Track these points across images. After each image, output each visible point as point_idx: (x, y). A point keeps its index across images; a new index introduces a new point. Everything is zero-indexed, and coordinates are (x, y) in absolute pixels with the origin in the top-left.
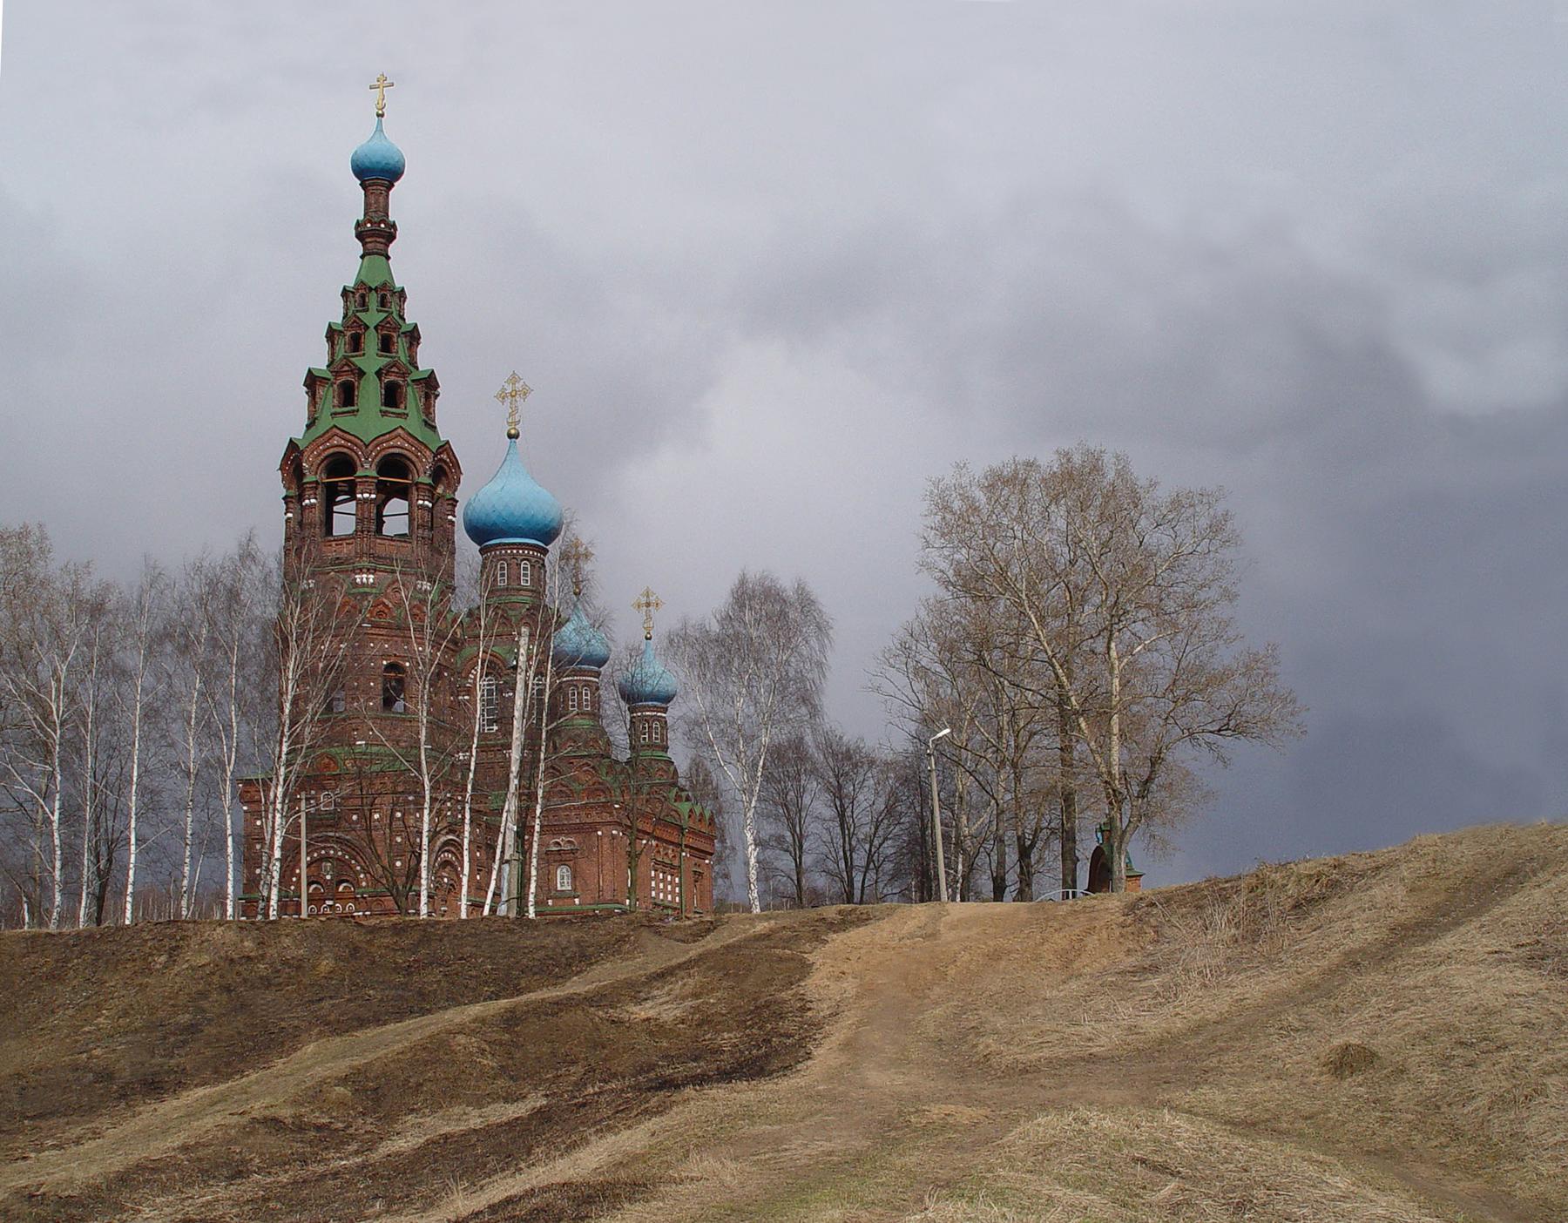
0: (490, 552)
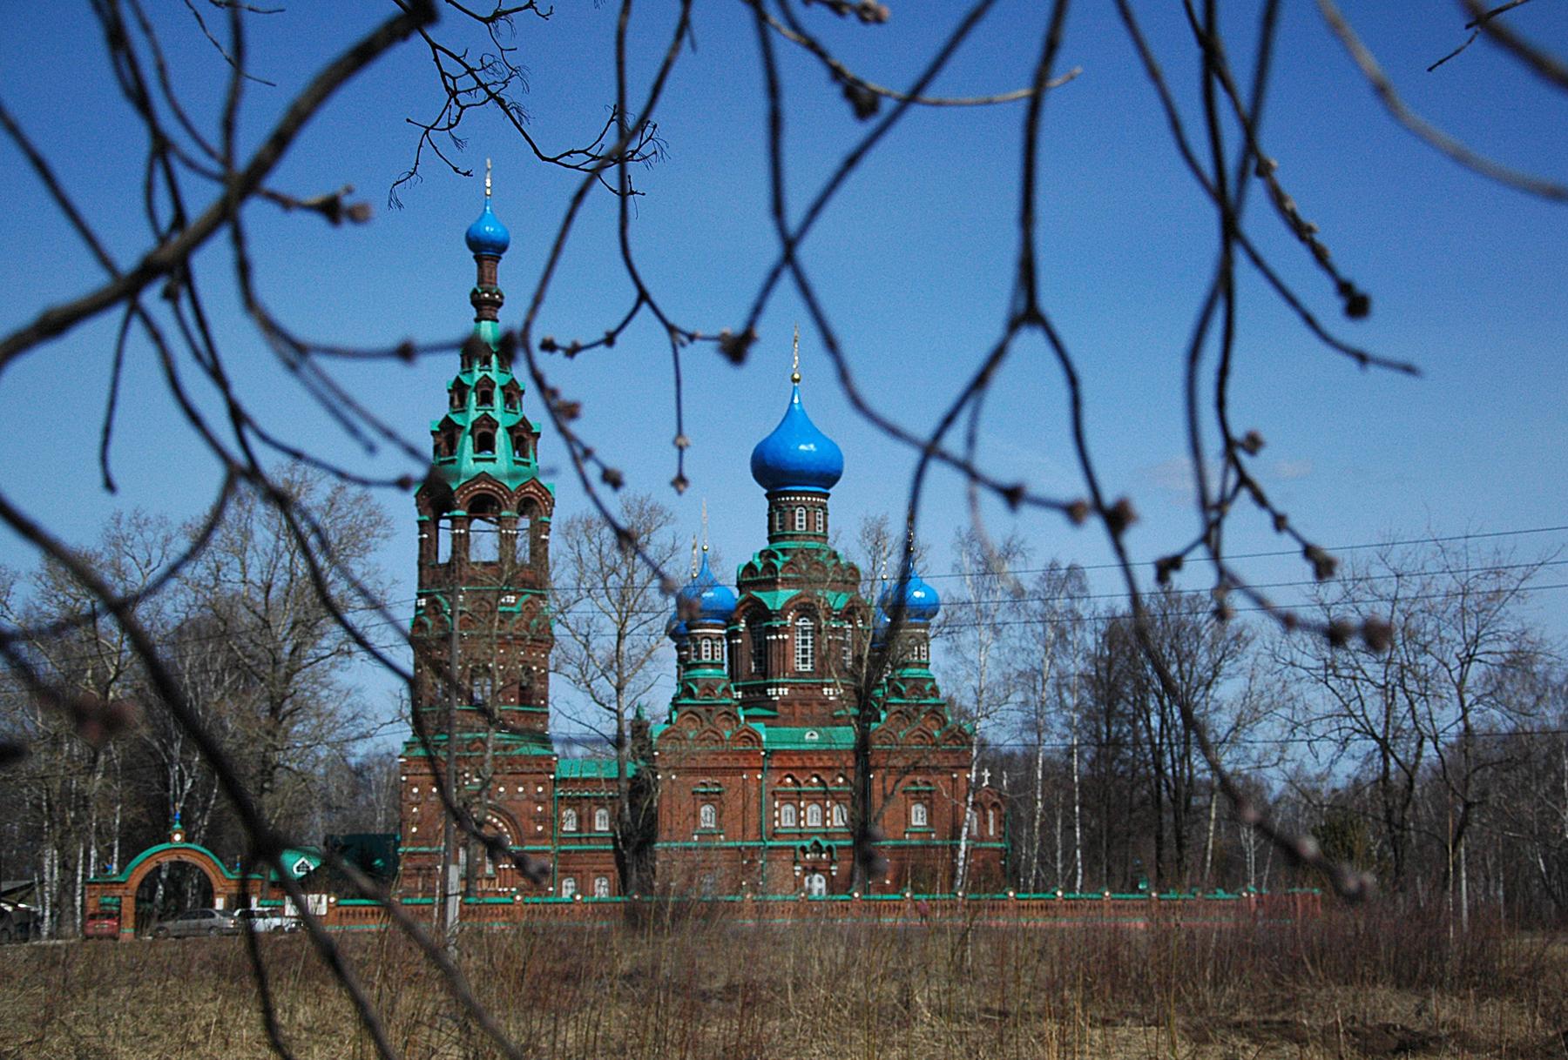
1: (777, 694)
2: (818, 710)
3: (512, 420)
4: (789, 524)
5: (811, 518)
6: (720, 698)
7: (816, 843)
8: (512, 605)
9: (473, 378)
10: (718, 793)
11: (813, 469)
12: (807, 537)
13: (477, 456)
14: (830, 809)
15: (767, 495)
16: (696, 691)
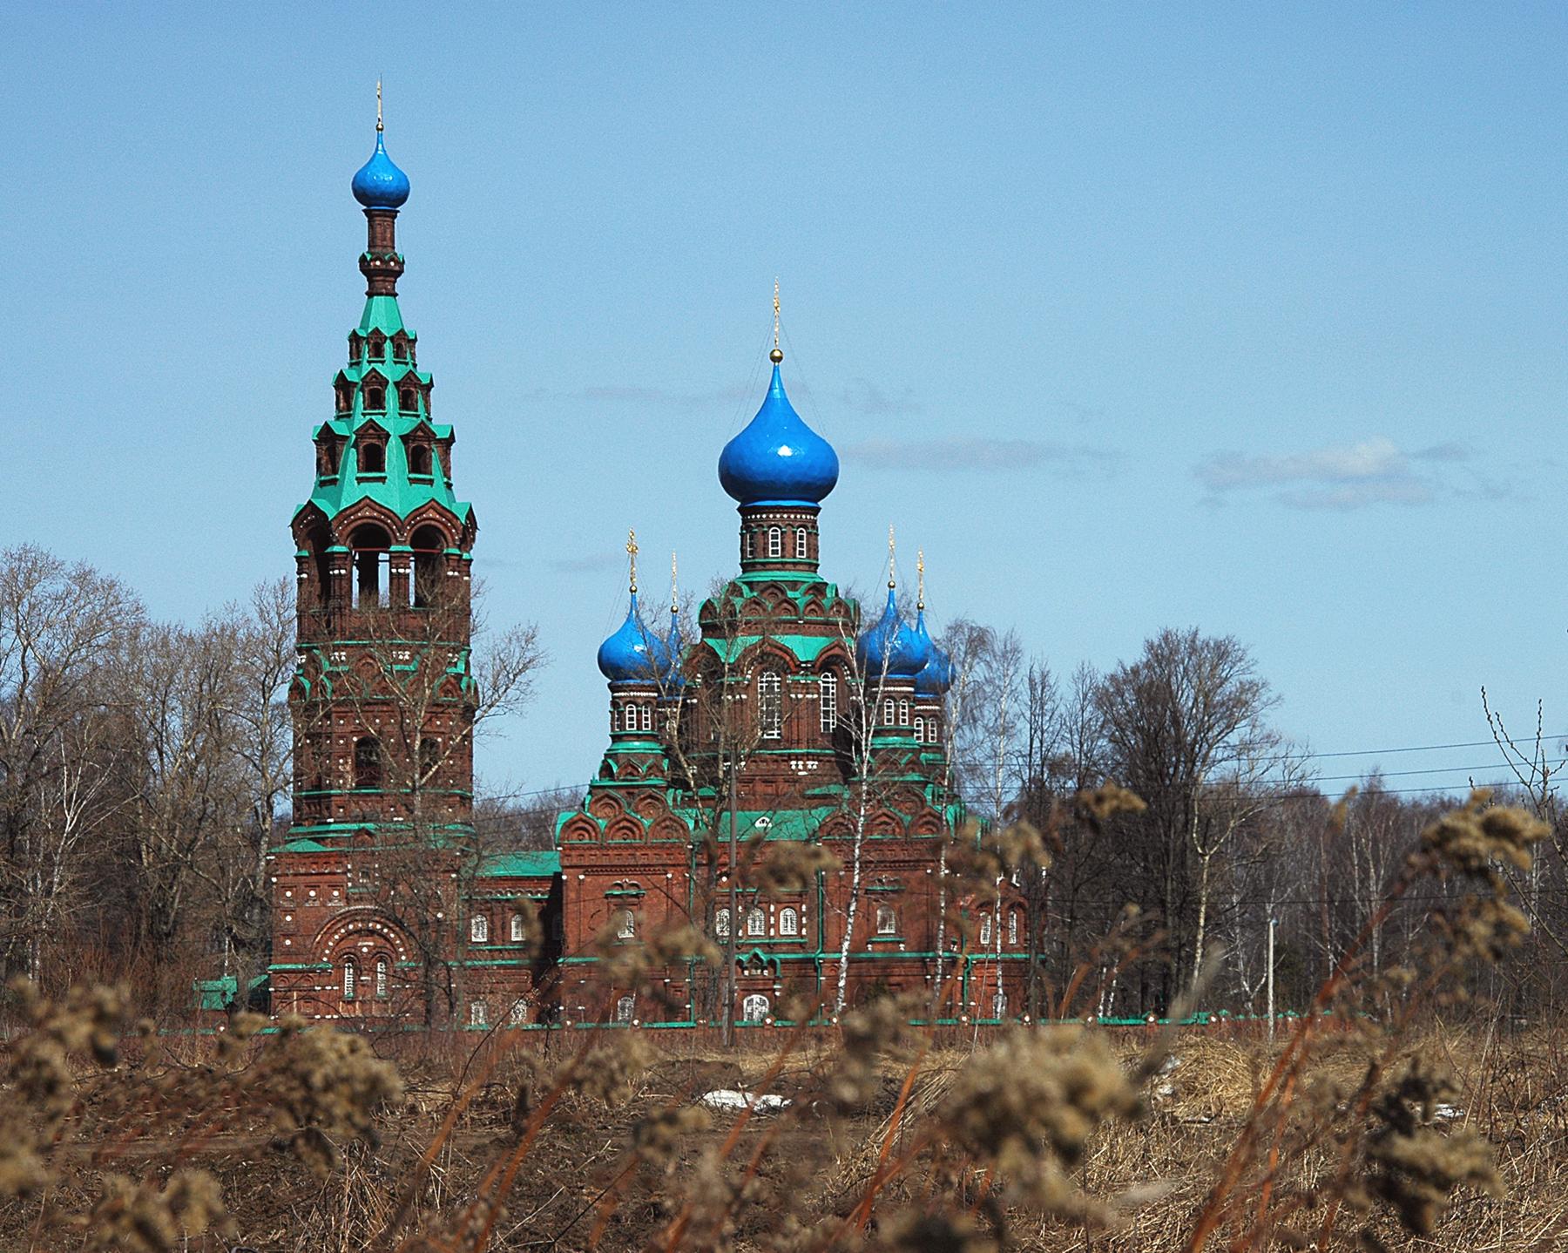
0: (761, 514)
1: (805, 768)
2: (784, 788)
3: (408, 425)
4: (760, 550)
5: (788, 540)
6: (644, 778)
7: (756, 956)
8: (406, 662)
9: (360, 373)
10: (636, 896)
11: (785, 479)
12: (783, 566)
13: (413, 476)
14: (776, 914)
15: (739, 510)
16: (615, 769)
